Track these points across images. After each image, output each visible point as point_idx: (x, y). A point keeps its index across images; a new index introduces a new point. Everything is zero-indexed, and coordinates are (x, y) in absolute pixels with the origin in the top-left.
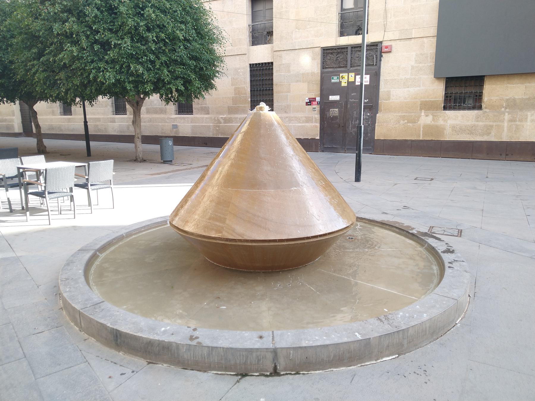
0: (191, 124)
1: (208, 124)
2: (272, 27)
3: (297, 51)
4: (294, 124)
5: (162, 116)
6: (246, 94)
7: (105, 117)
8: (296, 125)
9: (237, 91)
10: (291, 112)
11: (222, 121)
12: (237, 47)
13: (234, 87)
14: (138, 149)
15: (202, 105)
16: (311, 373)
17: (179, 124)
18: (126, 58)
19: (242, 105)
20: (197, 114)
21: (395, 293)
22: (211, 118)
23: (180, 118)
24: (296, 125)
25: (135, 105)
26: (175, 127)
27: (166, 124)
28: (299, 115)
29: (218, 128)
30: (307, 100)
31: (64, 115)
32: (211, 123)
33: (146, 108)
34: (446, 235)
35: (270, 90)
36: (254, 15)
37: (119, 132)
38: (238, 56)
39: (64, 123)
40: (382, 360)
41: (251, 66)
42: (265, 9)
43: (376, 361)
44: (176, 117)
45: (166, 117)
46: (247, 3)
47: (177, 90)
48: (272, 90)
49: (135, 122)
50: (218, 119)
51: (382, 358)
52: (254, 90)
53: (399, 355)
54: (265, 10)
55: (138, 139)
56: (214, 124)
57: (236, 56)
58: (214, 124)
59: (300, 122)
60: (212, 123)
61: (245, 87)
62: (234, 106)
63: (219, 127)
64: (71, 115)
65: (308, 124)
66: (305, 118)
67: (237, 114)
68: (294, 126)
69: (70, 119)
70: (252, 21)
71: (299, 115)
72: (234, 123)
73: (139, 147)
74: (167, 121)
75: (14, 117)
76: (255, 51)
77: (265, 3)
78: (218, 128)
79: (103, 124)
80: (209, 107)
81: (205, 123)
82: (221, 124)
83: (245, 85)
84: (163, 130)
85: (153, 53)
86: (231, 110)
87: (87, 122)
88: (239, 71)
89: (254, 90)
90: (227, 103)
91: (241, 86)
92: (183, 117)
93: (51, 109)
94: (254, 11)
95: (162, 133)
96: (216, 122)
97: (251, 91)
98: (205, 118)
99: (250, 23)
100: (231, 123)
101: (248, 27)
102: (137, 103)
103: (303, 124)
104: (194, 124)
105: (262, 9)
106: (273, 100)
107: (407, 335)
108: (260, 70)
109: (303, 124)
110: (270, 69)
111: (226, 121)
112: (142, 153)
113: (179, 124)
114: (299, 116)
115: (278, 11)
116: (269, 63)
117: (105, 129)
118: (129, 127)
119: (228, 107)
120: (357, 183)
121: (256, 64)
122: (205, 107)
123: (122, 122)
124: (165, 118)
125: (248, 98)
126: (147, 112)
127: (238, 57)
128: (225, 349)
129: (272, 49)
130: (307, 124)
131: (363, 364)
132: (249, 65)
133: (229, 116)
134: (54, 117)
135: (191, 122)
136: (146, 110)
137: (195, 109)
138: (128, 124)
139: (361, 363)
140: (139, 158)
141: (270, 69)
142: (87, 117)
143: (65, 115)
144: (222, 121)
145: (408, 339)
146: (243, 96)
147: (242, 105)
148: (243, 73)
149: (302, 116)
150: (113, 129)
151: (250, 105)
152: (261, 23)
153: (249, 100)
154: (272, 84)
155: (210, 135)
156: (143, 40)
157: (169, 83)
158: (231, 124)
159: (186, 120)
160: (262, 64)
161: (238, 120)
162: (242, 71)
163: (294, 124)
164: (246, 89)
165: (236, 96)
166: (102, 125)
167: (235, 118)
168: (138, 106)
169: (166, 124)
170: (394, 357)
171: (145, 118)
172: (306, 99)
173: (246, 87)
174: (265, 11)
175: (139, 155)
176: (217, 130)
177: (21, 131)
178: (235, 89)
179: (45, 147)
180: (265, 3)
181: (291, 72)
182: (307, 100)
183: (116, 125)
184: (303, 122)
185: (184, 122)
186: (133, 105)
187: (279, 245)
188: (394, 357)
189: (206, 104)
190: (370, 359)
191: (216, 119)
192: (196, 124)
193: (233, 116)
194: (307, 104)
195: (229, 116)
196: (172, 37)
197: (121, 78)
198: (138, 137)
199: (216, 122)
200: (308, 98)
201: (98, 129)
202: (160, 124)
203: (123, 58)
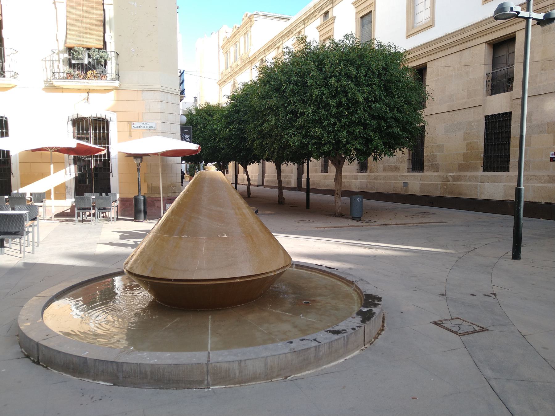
0: (421, 182)
1: (436, 182)
2: (513, 73)
3: (541, 96)
4: (533, 185)
5: (395, 173)
6: (478, 149)
7: (351, 174)
8: (536, 185)
9: (470, 146)
10: (531, 169)
11: (451, 179)
12: (471, 99)
13: (466, 142)
14: (337, 204)
15: (432, 162)
16: (84, 380)
17: (409, 182)
18: (312, 123)
19: (473, 162)
20: (427, 171)
21: (208, 346)
22: (440, 176)
23: (411, 175)
24: (536, 185)
25: (337, 164)
26: (405, 184)
27: (398, 182)
28: (541, 173)
29: (445, 187)
30: (552, 155)
31: (324, 173)
32: (439, 181)
33: (383, 166)
34: (447, 329)
35: (506, 144)
36: (495, 63)
37: (359, 189)
38: (473, 108)
39: (321, 180)
40: (97, 382)
41: (487, 118)
42: (508, 53)
43: (93, 381)
44: (407, 174)
45: (399, 175)
46: (486, 51)
47: (356, 149)
48: (509, 143)
49: (336, 180)
50: (447, 177)
51: (99, 380)
52: (488, 145)
53: (114, 385)
54: (508, 54)
55: (337, 195)
56: (442, 182)
57: (471, 108)
58: (442, 182)
59: (540, 182)
60: (441, 181)
61: (478, 142)
62: (465, 163)
63: (446, 185)
64: (328, 173)
65: (552, 185)
66: (547, 177)
67: (467, 172)
68: (532, 186)
69: (326, 176)
70: (493, 68)
71: (541, 173)
72: (462, 182)
73: (337, 203)
74: (399, 178)
75: (292, 175)
76: (492, 101)
77: (508, 46)
78: (445, 187)
79: (349, 181)
80: (439, 164)
81: (434, 181)
82: (449, 183)
83: (478, 139)
84: (394, 187)
85: (334, 116)
86: (462, 167)
87: (309, 179)
88: (473, 124)
89: (488, 145)
90: (458, 160)
91: (473, 141)
92: (414, 175)
93: (315, 168)
94: (495, 57)
95: (394, 190)
96: (444, 180)
97: (485, 146)
98: (434, 176)
99: (490, 70)
100: (460, 181)
101: (486, 76)
102: (339, 162)
103: (545, 185)
104: (423, 182)
105: (505, 54)
106: (509, 155)
107: (122, 370)
108: (496, 122)
109: (545, 185)
110: (508, 119)
111: (455, 179)
112: (340, 208)
113: (409, 182)
114: (541, 174)
115: (521, 53)
116: (506, 113)
117: (349, 185)
118: (367, 184)
119: (459, 164)
120: (513, 260)
121: (492, 116)
122: (435, 164)
123: (362, 179)
124: (398, 175)
125: (481, 154)
126: (384, 170)
127: (472, 110)
128: (139, 364)
129: (511, 97)
130: (550, 185)
131: (83, 379)
132: (484, 117)
133: (459, 174)
134: (316, 174)
135: (421, 180)
136: (383, 168)
137: (426, 166)
138: (367, 181)
139: (82, 377)
140: (338, 212)
141: (508, 119)
142: (310, 174)
143: (325, 173)
144: (451, 179)
145: (123, 374)
146: (475, 152)
147: (473, 162)
148: (477, 126)
149: (544, 174)
150: (355, 186)
151: (482, 161)
152: (502, 69)
153: (482, 155)
154: (510, 137)
155: (437, 193)
156: (327, 106)
157: (348, 143)
158: (459, 183)
159: (416, 177)
160: (499, 114)
161: (468, 178)
162: (476, 124)
163: (533, 185)
164: (479, 144)
165: (468, 152)
166: (348, 182)
167: (464, 176)
168: (340, 164)
169: (398, 182)
170: (108, 384)
171: (381, 175)
172: (551, 153)
173: (479, 141)
174: (508, 56)
175: (337, 210)
176: (445, 189)
177: (296, 186)
178: (467, 144)
179: (284, 199)
180: (508, 46)
181: (533, 122)
182: (552, 155)
183: (358, 182)
184: (545, 182)
185: (414, 180)
186: (335, 164)
187: (178, 284)
188: (108, 384)
189: (436, 161)
190: (88, 377)
191: (445, 177)
192: (425, 182)
193: (462, 174)
194: (552, 160)
195: (459, 174)
196: (355, 100)
197: (306, 141)
198: (338, 193)
199: (445, 180)
200: (553, 153)
201: (344, 186)
202: (393, 181)
203: (308, 123)
